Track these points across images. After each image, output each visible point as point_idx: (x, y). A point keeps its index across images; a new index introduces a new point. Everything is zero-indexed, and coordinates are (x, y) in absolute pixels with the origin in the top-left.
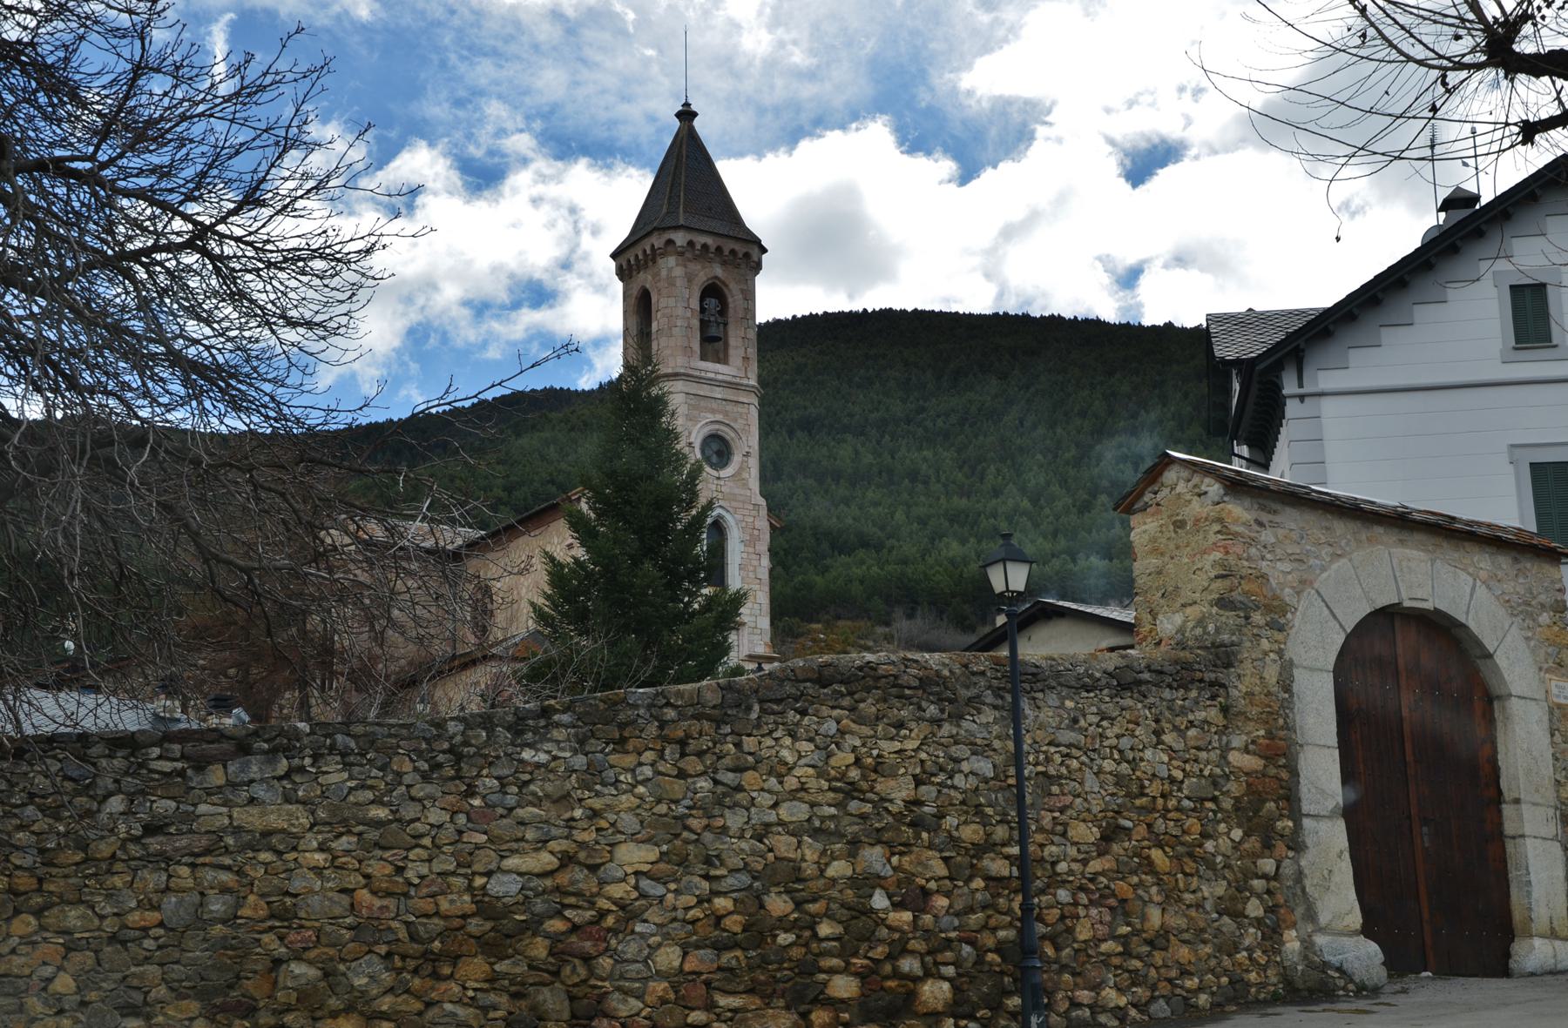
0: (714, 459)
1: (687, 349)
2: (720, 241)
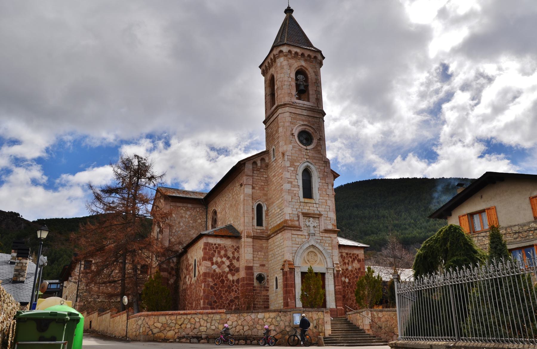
0: (304, 141)
1: (290, 94)
2: (303, 51)
